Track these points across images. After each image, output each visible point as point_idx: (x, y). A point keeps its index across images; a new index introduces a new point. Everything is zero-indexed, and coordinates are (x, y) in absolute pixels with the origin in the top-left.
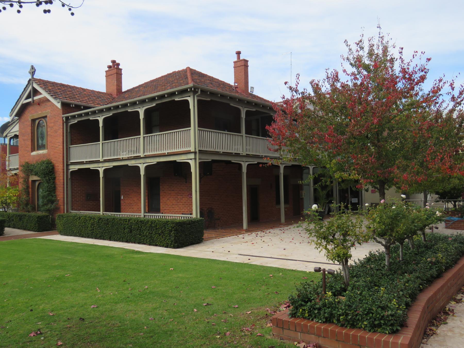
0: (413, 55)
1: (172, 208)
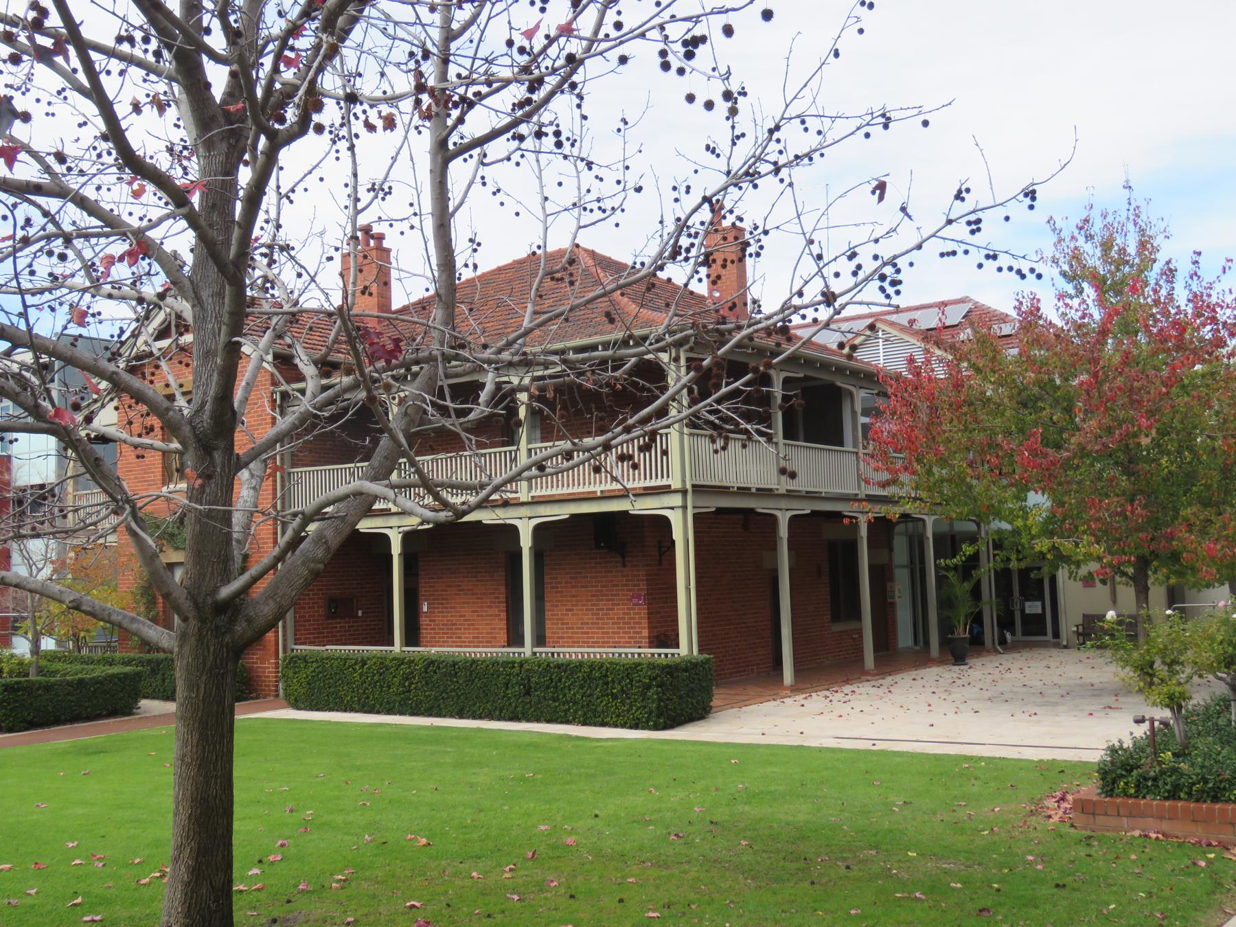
0: (1224, 268)
1: (583, 633)
